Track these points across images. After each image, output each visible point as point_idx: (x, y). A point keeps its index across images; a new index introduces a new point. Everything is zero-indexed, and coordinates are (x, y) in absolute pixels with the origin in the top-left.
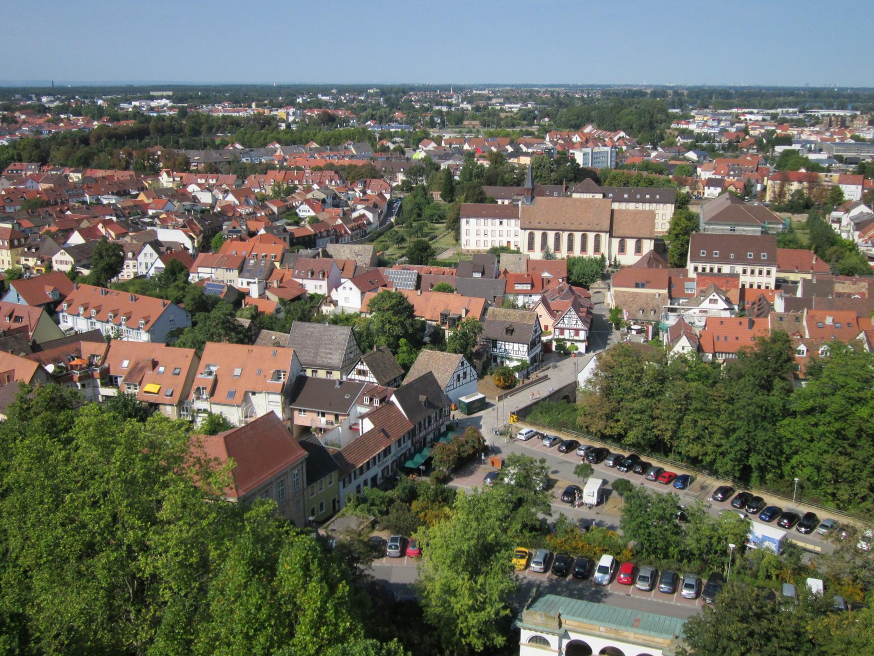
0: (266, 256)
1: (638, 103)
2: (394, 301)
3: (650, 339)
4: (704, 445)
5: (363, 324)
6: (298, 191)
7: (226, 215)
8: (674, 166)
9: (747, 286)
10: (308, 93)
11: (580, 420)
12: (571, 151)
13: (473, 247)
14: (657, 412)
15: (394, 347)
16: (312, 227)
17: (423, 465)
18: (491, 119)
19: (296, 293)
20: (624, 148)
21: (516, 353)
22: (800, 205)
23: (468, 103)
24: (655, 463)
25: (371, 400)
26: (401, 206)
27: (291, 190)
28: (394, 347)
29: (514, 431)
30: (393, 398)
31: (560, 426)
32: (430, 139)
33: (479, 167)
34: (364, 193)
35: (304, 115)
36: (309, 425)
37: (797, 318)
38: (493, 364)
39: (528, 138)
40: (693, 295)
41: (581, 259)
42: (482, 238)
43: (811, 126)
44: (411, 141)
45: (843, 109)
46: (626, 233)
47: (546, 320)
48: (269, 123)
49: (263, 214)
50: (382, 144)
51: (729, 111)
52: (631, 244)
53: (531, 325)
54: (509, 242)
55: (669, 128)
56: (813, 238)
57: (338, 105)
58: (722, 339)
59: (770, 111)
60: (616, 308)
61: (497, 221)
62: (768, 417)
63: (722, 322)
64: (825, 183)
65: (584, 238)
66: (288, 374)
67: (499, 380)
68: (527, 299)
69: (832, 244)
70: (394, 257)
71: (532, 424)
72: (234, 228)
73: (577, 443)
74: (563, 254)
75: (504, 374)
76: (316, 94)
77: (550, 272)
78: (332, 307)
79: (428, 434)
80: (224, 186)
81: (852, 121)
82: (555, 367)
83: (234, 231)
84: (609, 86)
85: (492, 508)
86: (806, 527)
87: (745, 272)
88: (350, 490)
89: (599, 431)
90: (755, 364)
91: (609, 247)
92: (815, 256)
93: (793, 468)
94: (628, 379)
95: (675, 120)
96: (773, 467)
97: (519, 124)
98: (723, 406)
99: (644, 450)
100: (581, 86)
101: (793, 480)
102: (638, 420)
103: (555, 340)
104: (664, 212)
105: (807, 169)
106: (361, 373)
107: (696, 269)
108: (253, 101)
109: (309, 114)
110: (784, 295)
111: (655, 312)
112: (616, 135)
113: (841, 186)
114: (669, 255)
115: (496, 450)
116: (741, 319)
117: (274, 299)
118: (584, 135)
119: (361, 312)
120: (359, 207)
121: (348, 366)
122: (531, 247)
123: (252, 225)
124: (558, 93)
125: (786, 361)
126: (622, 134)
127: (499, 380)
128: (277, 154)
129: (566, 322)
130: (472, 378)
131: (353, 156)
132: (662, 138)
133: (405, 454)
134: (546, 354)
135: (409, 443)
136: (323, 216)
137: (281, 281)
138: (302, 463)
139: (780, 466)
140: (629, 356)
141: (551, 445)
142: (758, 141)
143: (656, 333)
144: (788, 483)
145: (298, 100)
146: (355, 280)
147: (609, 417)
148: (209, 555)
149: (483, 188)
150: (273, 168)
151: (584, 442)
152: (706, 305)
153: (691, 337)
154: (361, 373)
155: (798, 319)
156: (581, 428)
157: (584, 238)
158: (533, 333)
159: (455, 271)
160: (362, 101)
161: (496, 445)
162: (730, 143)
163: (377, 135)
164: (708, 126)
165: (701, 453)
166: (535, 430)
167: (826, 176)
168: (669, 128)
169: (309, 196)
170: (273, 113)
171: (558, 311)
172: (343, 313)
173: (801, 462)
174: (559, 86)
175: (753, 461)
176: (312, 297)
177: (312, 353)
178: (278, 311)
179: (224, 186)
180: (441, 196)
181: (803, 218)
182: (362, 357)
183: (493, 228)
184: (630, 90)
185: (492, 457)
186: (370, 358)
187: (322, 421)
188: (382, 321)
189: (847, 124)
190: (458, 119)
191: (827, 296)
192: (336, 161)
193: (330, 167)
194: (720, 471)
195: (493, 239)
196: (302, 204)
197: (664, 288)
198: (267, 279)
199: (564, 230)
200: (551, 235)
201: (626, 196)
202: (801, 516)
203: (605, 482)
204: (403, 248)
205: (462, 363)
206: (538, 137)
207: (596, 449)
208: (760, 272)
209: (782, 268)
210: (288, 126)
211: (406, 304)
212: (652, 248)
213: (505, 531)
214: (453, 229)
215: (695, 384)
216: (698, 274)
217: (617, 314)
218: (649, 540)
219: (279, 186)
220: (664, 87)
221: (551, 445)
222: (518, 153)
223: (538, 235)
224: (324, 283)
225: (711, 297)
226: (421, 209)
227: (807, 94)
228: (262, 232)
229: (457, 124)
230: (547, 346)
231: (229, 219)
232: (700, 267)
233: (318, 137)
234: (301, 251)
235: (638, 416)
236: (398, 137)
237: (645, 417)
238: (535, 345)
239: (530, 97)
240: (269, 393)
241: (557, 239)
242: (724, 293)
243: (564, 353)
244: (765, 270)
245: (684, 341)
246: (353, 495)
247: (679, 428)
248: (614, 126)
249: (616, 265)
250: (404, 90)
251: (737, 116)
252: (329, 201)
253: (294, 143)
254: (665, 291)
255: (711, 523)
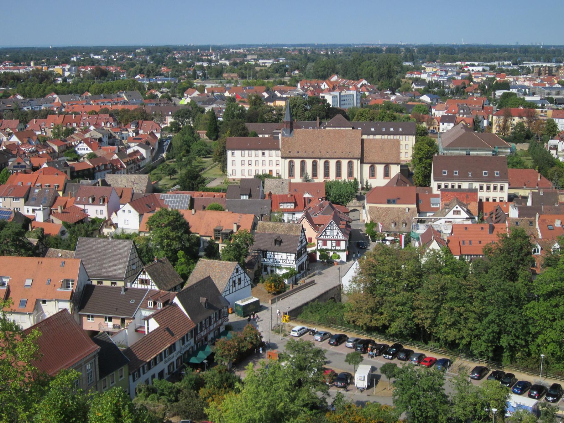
0: (49, 186)
1: (376, 58)
2: (171, 218)
3: (403, 247)
4: (460, 330)
5: (143, 242)
6: (76, 132)
7: (11, 154)
8: (412, 106)
9: (484, 200)
10: (81, 53)
11: (347, 316)
12: (321, 95)
13: (238, 176)
14: (417, 303)
15: (174, 259)
16: (91, 162)
17: (206, 359)
18: (247, 72)
19: (79, 217)
20: (367, 93)
21: (286, 261)
22: (522, 135)
23: (226, 59)
24: (416, 350)
25: (155, 304)
26: (171, 144)
27: (70, 132)
28: (174, 259)
29: (287, 329)
30: (176, 300)
31: (329, 323)
32: (194, 88)
33: (240, 109)
34: (137, 133)
35: (79, 71)
36: (97, 329)
37: (531, 222)
38: (264, 273)
39: (283, 87)
40: (438, 208)
41: (336, 183)
42: (247, 168)
43: (524, 75)
44: (177, 90)
45: (549, 62)
46: (376, 159)
47: (310, 233)
48: (46, 78)
49: (45, 152)
50: (151, 93)
51: (455, 64)
52: (380, 169)
53: (298, 236)
54: (271, 171)
55: (404, 78)
56: (536, 161)
57: (110, 63)
58: (467, 243)
59: (489, 64)
60: (372, 222)
61: (260, 152)
62: (515, 301)
63: (466, 229)
64: (541, 118)
65: (338, 165)
66: (76, 283)
67: (271, 287)
68: (291, 217)
69: (552, 166)
70: (167, 186)
71: (303, 322)
72: (19, 163)
73: (345, 336)
74: (321, 178)
75: (275, 281)
76: (88, 54)
77: (310, 193)
78: (112, 230)
79: (209, 333)
80: (8, 130)
81: (557, 70)
82: (320, 274)
83: (19, 166)
84: (350, 45)
85: (280, 380)
86: (553, 396)
87: (481, 188)
88: (140, 383)
89: (365, 324)
90: (499, 258)
91: (361, 172)
92: (539, 174)
93: (538, 346)
94: (390, 275)
95: (409, 72)
96: (522, 346)
97: (273, 76)
98: (475, 294)
99: (407, 340)
100: (325, 45)
101: (540, 356)
102: (401, 312)
103: (319, 250)
104: (407, 143)
105: (524, 107)
106: (143, 282)
107: (439, 187)
108: (31, 60)
109: (83, 70)
110: (517, 205)
111: (406, 224)
112: (359, 83)
113: (554, 119)
114: (414, 177)
115: (273, 346)
116: (482, 225)
117: (58, 222)
118: (331, 83)
119: (140, 232)
120: (132, 145)
121: (132, 275)
122: (291, 174)
123: (35, 162)
124: (306, 51)
125: (526, 255)
126: (364, 82)
127: (271, 287)
128: (56, 101)
129: (328, 234)
130: (247, 284)
131: (125, 103)
132: (398, 85)
133: (188, 351)
134: (312, 263)
135: (192, 341)
136: (100, 153)
137: (64, 207)
138: (95, 356)
139: (527, 345)
140: (390, 255)
141: (322, 340)
142: (481, 87)
143: (408, 242)
144: (535, 360)
145: (72, 59)
146: (132, 203)
147: (374, 311)
148: (18, 417)
149: (246, 125)
150: (53, 113)
151: (352, 335)
152: (450, 215)
153: (440, 242)
154: (143, 282)
155: (531, 223)
156: (349, 323)
157: (338, 165)
158: (299, 243)
159: (224, 194)
160: (131, 59)
161: (272, 341)
162: (458, 89)
163: (146, 86)
164: (437, 75)
165: (458, 337)
166: (306, 327)
167: (542, 112)
168: (404, 78)
169: (87, 136)
170: (50, 69)
171: (320, 225)
172: (123, 233)
173: (545, 340)
174: (305, 45)
175: (504, 341)
176: (94, 221)
177: (97, 265)
178: (63, 233)
179: (8, 130)
180: (207, 135)
181: (524, 147)
182: (144, 267)
183: (256, 158)
184: (367, 48)
185: (269, 351)
186: (152, 268)
187: (110, 326)
188: (161, 237)
189: (554, 73)
190: (218, 73)
191: (554, 205)
192: (109, 106)
193: (106, 111)
194: (475, 352)
195: (257, 168)
196: (80, 142)
197: (413, 204)
198: (51, 206)
199: (320, 158)
200: (309, 163)
201: (373, 129)
202: (548, 388)
203: (373, 369)
204: (175, 179)
205: (237, 271)
206: (290, 85)
207: (363, 340)
208: (495, 188)
209: (512, 186)
210: (65, 80)
211: (182, 221)
212: (399, 171)
213: (293, 400)
214: (220, 161)
215: (449, 276)
216: (442, 190)
217: (373, 227)
218: (420, 410)
219: (58, 129)
220: (396, 45)
221: (322, 340)
222: (273, 98)
223: (297, 163)
224: (104, 208)
225: (455, 209)
226: (189, 146)
227: (518, 50)
228: (45, 165)
229: (217, 77)
230: (312, 257)
231: (14, 156)
232: (443, 185)
233: (93, 87)
234: (81, 181)
235: (400, 308)
236: (165, 87)
237: (406, 308)
238: (302, 255)
239: (281, 54)
240: (58, 301)
241: (315, 165)
242: (465, 206)
243: (328, 262)
244: (499, 185)
245: (434, 245)
246: (143, 386)
247: (437, 316)
248: (357, 75)
249: (368, 188)
250: (168, 50)
251: (461, 67)
252: (105, 140)
253: (71, 93)
254: (414, 206)
255: (474, 391)
